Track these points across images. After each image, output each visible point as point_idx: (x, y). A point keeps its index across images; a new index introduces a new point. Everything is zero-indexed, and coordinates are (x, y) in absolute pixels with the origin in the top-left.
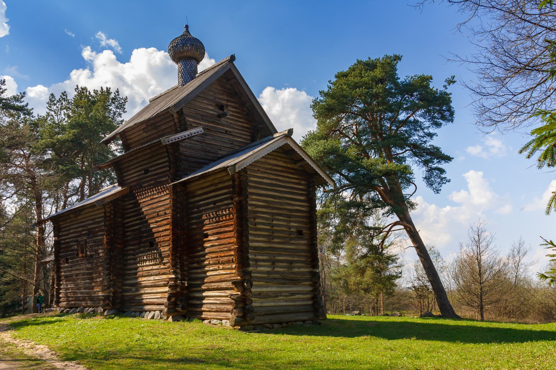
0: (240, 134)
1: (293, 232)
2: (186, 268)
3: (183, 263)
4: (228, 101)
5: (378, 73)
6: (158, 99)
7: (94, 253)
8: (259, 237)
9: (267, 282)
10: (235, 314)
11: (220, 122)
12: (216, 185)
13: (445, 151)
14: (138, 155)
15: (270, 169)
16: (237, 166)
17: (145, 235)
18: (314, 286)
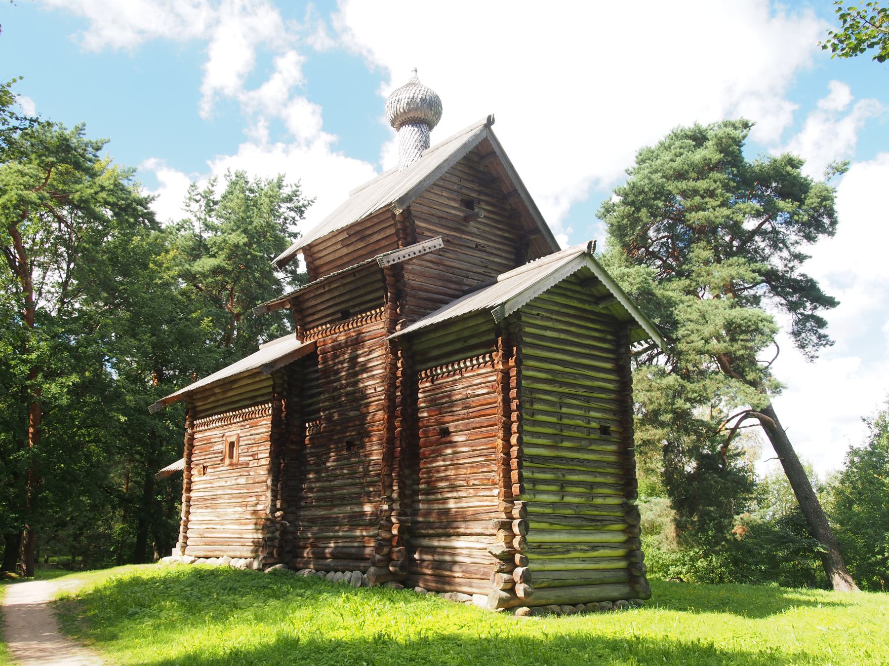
0: (499, 249)
1: (593, 428)
2: (408, 492)
3: (404, 483)
4: (480, 193)
5: (708, 152)
6: (364, 191)
7: (251, 458)
8: (539, 437)
9: (551, 524)
10: (498, 583)
11: (467, 229)
12: (465, 339)
13: (826, 289)
14: (333, 286)
15: (558, 313)
16: (506, 306)
17: (339, 428)
18: (629, 533)
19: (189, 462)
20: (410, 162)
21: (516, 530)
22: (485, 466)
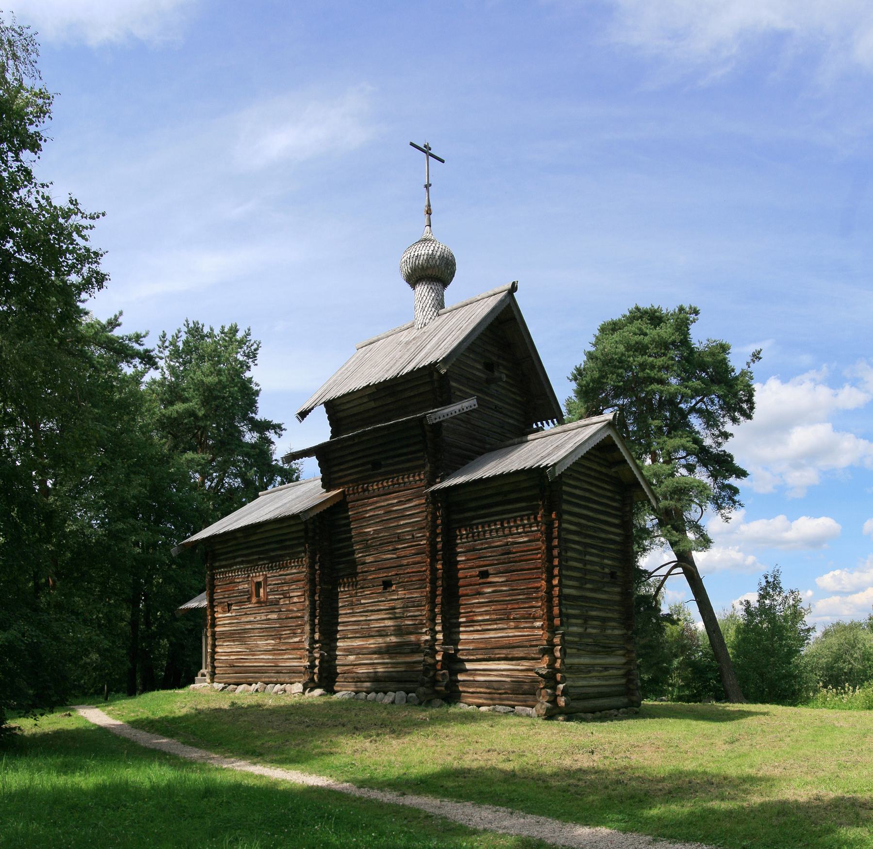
5: (665, 332)
7: (282, 596)
10: (543, 697)
13: (738, 462)
16: (557, 467)
19: (211, 601)
20: (428, 320)
21: (558, 654)
22: (525, 603)
